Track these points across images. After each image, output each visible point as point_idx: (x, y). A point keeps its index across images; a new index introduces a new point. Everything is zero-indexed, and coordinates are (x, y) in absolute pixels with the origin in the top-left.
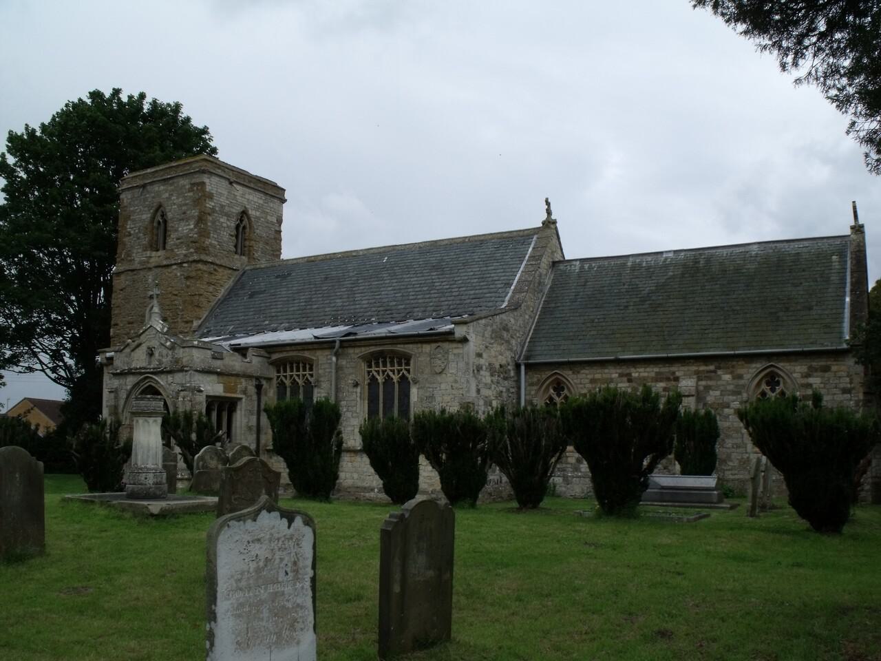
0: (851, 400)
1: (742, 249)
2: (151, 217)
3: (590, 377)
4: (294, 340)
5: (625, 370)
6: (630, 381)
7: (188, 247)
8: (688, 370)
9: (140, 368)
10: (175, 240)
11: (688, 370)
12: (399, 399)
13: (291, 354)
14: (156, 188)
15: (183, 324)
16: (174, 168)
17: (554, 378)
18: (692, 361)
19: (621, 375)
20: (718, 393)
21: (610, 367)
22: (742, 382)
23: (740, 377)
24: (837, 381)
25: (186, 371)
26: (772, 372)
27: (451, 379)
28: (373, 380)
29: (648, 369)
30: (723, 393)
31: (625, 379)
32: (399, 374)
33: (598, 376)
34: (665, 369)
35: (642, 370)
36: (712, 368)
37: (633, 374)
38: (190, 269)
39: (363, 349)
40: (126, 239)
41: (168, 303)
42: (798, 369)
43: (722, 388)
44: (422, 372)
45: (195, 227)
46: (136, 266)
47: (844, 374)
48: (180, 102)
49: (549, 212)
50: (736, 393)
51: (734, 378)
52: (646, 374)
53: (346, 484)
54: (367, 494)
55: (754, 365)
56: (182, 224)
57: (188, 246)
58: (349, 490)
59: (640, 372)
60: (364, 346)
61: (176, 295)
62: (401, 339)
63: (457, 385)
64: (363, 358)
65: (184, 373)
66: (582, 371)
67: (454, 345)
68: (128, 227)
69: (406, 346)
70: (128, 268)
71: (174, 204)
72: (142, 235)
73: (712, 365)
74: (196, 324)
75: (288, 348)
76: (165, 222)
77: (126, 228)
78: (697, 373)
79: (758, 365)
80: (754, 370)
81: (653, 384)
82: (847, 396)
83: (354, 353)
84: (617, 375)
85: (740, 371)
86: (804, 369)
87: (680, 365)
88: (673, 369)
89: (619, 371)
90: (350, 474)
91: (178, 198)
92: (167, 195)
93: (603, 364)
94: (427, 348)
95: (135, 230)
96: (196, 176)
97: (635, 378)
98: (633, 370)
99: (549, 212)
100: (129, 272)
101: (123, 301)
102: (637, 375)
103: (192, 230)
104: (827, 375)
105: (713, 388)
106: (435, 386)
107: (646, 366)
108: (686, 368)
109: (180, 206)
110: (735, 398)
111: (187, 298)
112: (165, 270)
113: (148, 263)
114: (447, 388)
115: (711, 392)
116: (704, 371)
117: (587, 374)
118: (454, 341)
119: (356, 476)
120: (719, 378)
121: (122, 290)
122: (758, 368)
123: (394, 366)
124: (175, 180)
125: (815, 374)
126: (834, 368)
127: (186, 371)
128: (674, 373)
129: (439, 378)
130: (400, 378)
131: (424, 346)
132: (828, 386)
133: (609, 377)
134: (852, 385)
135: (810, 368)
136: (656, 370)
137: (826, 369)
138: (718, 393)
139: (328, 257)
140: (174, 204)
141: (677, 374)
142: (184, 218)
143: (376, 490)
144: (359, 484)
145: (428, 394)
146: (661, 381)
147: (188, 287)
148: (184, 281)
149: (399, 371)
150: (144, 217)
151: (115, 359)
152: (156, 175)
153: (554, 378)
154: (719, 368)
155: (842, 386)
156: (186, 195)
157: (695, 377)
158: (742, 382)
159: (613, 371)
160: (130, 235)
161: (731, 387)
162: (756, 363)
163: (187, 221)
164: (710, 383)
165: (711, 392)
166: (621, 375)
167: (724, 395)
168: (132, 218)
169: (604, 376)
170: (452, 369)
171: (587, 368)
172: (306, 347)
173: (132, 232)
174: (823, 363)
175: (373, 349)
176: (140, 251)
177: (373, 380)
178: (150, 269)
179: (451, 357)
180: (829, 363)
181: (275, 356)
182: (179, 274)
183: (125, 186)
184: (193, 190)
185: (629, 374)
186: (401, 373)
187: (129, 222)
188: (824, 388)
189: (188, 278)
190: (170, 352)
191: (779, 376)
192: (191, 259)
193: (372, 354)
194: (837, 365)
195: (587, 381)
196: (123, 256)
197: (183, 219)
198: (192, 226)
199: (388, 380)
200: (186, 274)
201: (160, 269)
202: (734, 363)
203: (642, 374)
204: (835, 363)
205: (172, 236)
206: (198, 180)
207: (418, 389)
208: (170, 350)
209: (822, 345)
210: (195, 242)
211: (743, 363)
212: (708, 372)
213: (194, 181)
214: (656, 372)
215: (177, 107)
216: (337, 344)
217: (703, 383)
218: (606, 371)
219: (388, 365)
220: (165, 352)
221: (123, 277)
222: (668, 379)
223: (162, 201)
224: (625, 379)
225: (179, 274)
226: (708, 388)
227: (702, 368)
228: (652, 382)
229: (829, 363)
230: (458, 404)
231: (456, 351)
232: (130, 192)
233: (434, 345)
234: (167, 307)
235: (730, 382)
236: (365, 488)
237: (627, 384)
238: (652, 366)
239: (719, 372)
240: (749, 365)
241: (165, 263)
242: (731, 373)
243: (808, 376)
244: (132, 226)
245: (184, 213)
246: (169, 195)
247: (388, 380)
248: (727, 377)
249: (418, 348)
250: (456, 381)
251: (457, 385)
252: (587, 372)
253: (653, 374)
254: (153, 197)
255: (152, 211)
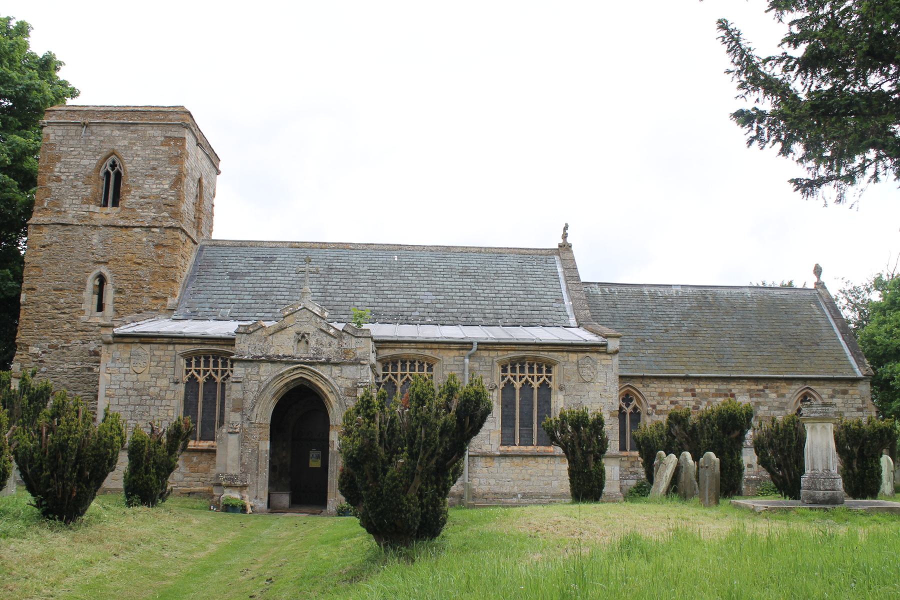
0: (863, 416)
1: (635, 289)
2: (97, 164)
3: (659, 390)
4: (416, 337)
5: (689, 385)
6: (694, 395)
7: (159, 209)
8: (742, 389)
9: (284, 356)
10: (137, 198)
11: (742, 389)
12: (538, 405)
13: (407, 351)
14: (107, 131)
15: (150, 299)
16: (138, 114)
17: (626, 389)
18: (745, 381)
19: (686, 390)
20: (766, 408)
21: (676, 383)
22: (784, 400)
23: (783, 396)
24: (853, 402)
25: (362, 365)
26: (807, 392)
27: (601, 388)
28: (193, 379)
29: (709, 386)
30: (770, 408)
31: (690, 393)
32: (205, 374)
33: (665, 390)
34: (723, 386)
35: (704, 386)
36: (761, 387)
37: (697, 390)
38: (163, 236)
39: (500, 353)
40: (53, 185)
41: (125, 272)
42: (825, 391)
43: (769, 404)
44: (569, 380)
45: (171, 188)
46: (69, 219)
47: (858, 397)
48: (28, 21)
49: (565, 236)
50: (781, 408)
51: (778, 397)
52: (707, 390)
53: (480, 491)
54: (509, 500)
55: (793, 387)
56: (150, 181)
57: (159, 208)
58: (486, 496)
59: (702, 389)
60: (391, 348)
61: (139, 264)
62: (548, 347)
63: (606, 394)
64: (184, 355)
65: (359, 367)
66: (652, 385)
67: (604, 356)
68: (56, 170)
69: (550, 353)
70: (55, 220)
71: (138, 155)
72: (80, 183)
73: (760, 385)
74: (171, 302)
75: (406, 345)
76: (118, 176)
77: (52, 171)
78: (749, 391)
79: (797, 387)
80: (794, 391)
81: (714, 399)
82: (861, 413)
83: (489, 356)
84: (683, 390)
85: (783, 391)
86: (830, 392)
87: (735, 384)
88: (730, 387)
89: (684, 386)
90: (485, 480)
91: (143, 149)
92: (126, 143)
93: (669, 379)
94: (574, 357)
95: (68, 176)
96: (173, 129)
97: (699, 393)
98: (696, 386)
99: (565, 236)
100: (59, 227)
101: (45, 261)
102: (700, 390)
103: (166, 190)
104: (846, 396)
105: (762, 403)
106: (583, 394)
107: (707, 383)
108: (739, 387)
109: (145, 159)
110: (779, 412)
111: (157, 270)
112: (124, 232)
113: (91, 219)
114: (596, 396)
115: (761, 407)
116: (754, 389)
117: (656, 388)
118: (606, 353)
119: (492, 482)
120: (767, 396)
121: (44, 247)
122: (797, 390)
123: (533, 372)
124: (139, 128)
125: (838, 396)
126: (851, 392)
127: (362, 365)
128: (730, 390)
129: (587, 387)
130: (541, 385)
131: (571, 355)
132: (847, 406)
133: (676, 391)
134: (864, 406)
135: (834, 390)
136: (716, 387)
137: (845, 392)
138: (766, 408)
139: (341, 246)
140: (138, 155)
141: (733, 391)
142: (153, 173)
143: (519, 496)
144: (497, 490)
145: (576, 401)
146: (720, 397)
147: (159, 256)
148: (152, 249)
149: (205, 372)
150: (85, 162)
151: (237, 341)
152: (109, 116)
153: (626, 389)
154: (767, 388)
155: (857, 406)
156: (158, 148)
157: (748, 394)
158: (784, 400)
159: (679, 386)
160: (58, 179)
161: (776, 404)
162: (795, 384)
163: (156, 179)
164: (760, 400)
165: (761, 407)
166: (686, 390)
167: (771, 410)
168: (62, 160)
169: (671, 390)
170: (601, 378)
171: (656, 382)
172: (429, 346)
173: (63, 177)
174: (843, 388)
175: (513, 354)
176: (77, 202)
177: (192, 381)
178: (95, 227)
179: (599, 367)
180: (847, 388)
181: (387, 353)
182: (144, 239)
183: (53, 119)
184: (170, 145)
185: (693, 390)
186: (190, 373)
187: (58, 165)
188: (845, 406)
189: (157, 246)
190: (335, 341)
191: (811, 396)
192: (165, 224)
193: (195, 352)
194: (853, 390)
195: (655, 394)
196: (45, 204)
197: (151, 176)
198: (167, 187)
199: (527, 385)
200: (156, 241)
201: (112, 229)
202: (778, 384)
203: (704, 390)
204: (851, 388)
205: (132, 192)
206: (176, 135)
207: (564, 396)
208: (335, 338)
209: (842, 373)
210: (169, 205)
211: (785, 384)
212: (758, 390)
213: (169, 134)
214: (716, 389)
215: (23, 29)
216: (475, 347)
217: (755, 399)
218: (673, 386)
219: (527, 370)
220: (326, 340)
221: (46, 230)
222: (726, 395)
223: (116, 148)
224: (690, 393)
225: (144, 239)
226: (758, 404)
227: (754, 387)
228: (713, 397)
229: (847, 388)
230: (608, 412)
231: (604, 362)
232: (62, 128)
233: (581, 355)
234: (125, 277)
235: (776, 400)
236: (506, 494)
237: (692, 398)
238: (712, 383)
239: (767, 391)
240: (790, 387)
241: (121, 223)
242: (776, 392)
243: (832, 397)
244: (63, 170)
245: (154, 169)
246: (130, 143)
247: (527, 385)
248: (774, 395)
249: (563, 357)
250: (605, 391)
251: (606, 394)
252: (656, 386)
253: (713, 391)
254: (102, 141)
255: (98, 158)
